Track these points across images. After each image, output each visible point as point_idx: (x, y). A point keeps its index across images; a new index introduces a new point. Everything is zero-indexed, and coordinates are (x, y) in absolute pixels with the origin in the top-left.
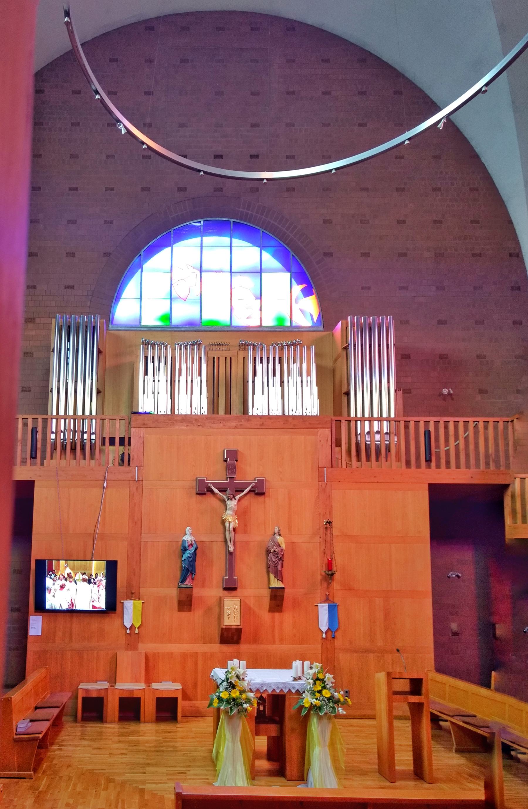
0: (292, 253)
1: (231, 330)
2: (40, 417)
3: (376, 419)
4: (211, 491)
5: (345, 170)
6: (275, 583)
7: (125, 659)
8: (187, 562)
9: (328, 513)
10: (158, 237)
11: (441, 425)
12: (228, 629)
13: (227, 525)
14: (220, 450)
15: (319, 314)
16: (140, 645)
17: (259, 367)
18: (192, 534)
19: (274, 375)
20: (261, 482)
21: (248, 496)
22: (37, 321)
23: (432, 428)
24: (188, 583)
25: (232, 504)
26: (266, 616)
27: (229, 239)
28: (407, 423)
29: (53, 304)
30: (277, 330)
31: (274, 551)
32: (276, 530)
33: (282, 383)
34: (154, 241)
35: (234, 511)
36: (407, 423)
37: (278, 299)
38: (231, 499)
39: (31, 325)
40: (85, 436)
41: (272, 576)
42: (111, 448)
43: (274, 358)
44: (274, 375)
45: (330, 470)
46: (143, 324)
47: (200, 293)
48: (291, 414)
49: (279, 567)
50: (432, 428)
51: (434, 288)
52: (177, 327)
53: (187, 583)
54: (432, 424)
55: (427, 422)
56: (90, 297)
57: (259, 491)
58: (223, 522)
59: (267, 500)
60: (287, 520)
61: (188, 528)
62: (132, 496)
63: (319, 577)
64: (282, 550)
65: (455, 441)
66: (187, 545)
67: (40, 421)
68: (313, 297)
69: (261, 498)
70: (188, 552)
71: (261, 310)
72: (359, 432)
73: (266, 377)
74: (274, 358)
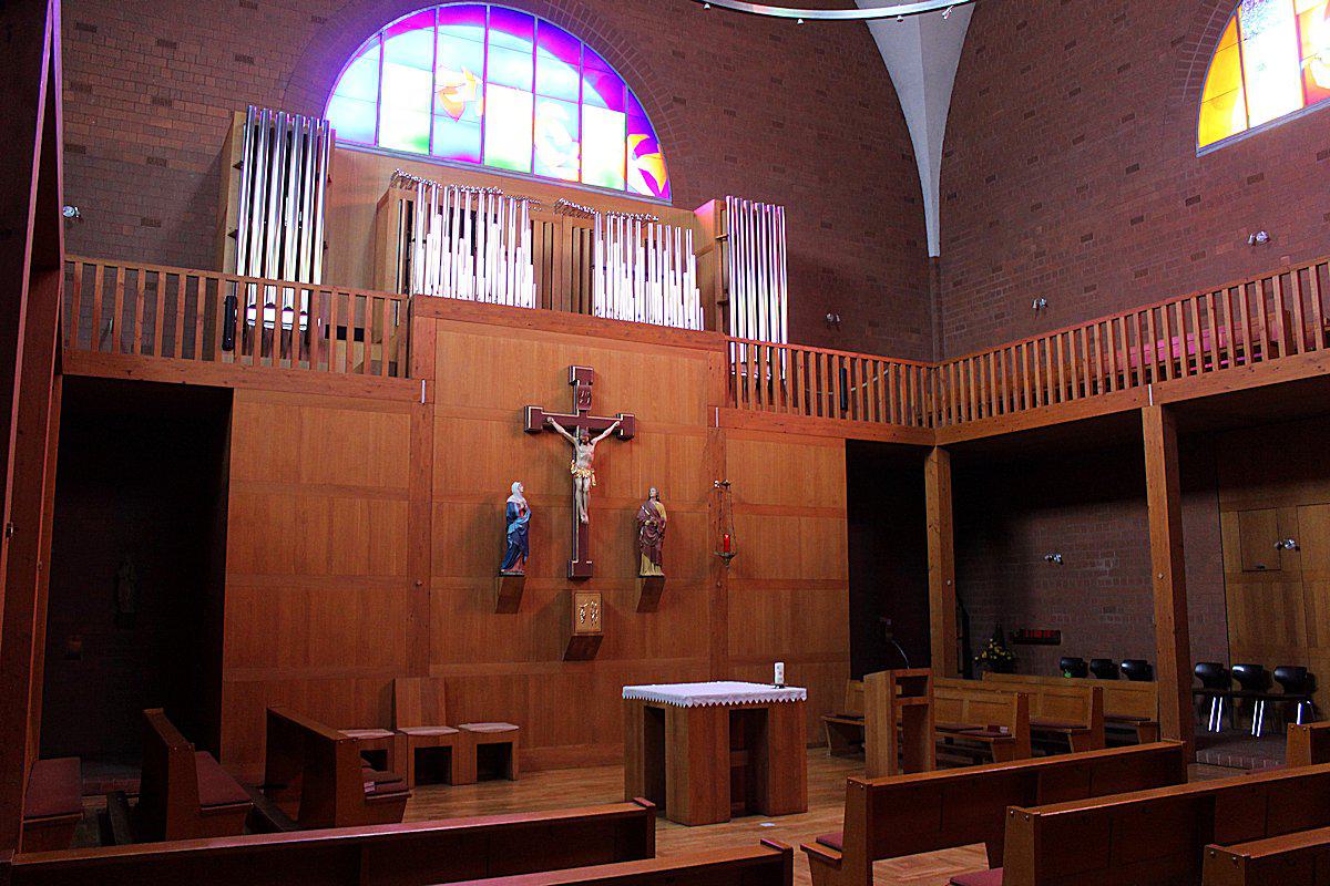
0: (627, 87)
1: (578, 190)
2: (203, 276)
3: (742, 341)
4: (552, 430)
5: (840, 23)
6: (650, 570)
7: (410, 691)
8: (516, 536)
9: (720, 471)
10: (414, 13)
11: (858, 363)
12: (583, 637)
13: (579, 482)
14: (562, 366)
15: (667, 183)
16: (432, 668)
17: (436, 220)
18: (524, 495)
19: (462, 235)
20: (629, 421)
21: (607, 441)
22: (177, 105)
23: (847, 366)
24: (516, 569)
25: (585, 451)
26: (632, 617)
27: (483, 30)
28: (794, 352)
29: (211, 81)
30: (605, 192)
31: (652, 523)
32: (653, 493)
33: (474, 252)
34: (405, 17)
35: (590, 461)
36: (794, 352)
37: (601, 149)
38: (585, 444)
39: (163, 111)
40: (252, 314)
41: (646, 560)
42: (342, 343)
43: (462, 212)
44: (462, 235)
45: (724, 410)
46: (382, 144)
47: (480, 114)
48: (428, 292)
49: (658, 546)
50: (847, 366)
51: (816, 178)
52: (438, 158)
53: (514, 569)
54: (848, 360)
55: (842, 358)
56: (285, 84)
57: (625, 435)
58: (573, 477)
59: (635, 448)
60: (662, 481)
61: (516, 485)
62: (415, 427)
63: (708, 561)
64: (662, 522)
65: (876, 382)
66: (517, 509)
67: (202, 282)
68: (658, 155)
69: (626, 445)
70: (519, 520)
71: (580, 158)
72: (733, 361)
73: (448, 238)
74: (462, 212)
